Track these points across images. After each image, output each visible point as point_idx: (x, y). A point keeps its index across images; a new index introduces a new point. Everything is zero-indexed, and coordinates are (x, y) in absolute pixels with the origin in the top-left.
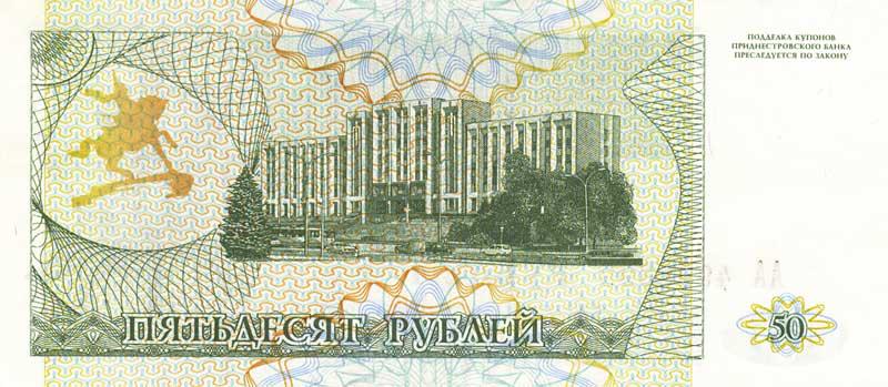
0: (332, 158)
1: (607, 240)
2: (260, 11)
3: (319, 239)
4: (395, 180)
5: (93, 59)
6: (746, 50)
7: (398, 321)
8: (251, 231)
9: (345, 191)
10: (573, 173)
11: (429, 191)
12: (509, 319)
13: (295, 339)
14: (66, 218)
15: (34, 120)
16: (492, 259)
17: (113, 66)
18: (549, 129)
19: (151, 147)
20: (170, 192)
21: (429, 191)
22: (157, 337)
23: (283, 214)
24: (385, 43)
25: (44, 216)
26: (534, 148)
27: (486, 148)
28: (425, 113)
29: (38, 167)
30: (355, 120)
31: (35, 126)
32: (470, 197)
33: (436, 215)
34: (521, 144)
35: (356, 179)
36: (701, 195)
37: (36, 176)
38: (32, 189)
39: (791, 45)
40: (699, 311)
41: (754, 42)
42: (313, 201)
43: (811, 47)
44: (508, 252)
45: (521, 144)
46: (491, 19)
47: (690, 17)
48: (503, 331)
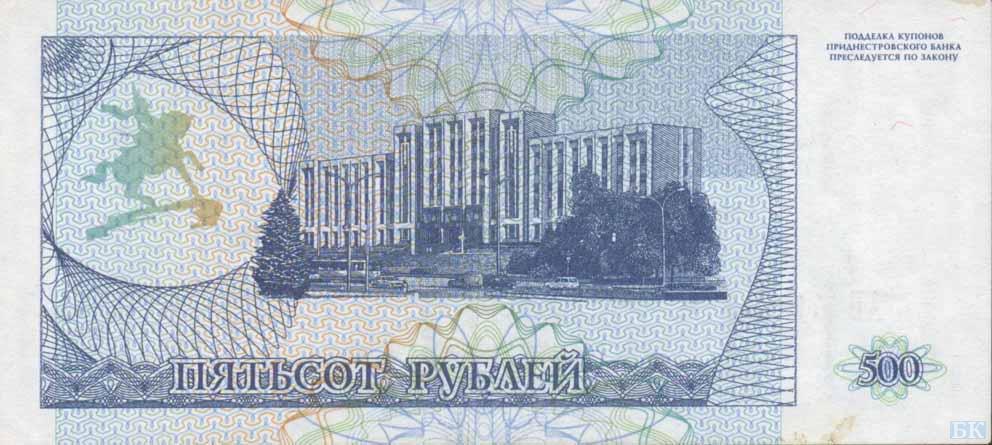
3: (364, 272)
4: (448, 204)
8: (288, 265)
10: (649, 192)
15: (45, 137)
16: (556, 293)
18: (621, 145)
19: (174, 170)
20: (196, 221)
26: (604, 166)
27: (550, 167)
28: (482, 126)
32: (534, 223)
34: (590, 162)
45: (590, 162)
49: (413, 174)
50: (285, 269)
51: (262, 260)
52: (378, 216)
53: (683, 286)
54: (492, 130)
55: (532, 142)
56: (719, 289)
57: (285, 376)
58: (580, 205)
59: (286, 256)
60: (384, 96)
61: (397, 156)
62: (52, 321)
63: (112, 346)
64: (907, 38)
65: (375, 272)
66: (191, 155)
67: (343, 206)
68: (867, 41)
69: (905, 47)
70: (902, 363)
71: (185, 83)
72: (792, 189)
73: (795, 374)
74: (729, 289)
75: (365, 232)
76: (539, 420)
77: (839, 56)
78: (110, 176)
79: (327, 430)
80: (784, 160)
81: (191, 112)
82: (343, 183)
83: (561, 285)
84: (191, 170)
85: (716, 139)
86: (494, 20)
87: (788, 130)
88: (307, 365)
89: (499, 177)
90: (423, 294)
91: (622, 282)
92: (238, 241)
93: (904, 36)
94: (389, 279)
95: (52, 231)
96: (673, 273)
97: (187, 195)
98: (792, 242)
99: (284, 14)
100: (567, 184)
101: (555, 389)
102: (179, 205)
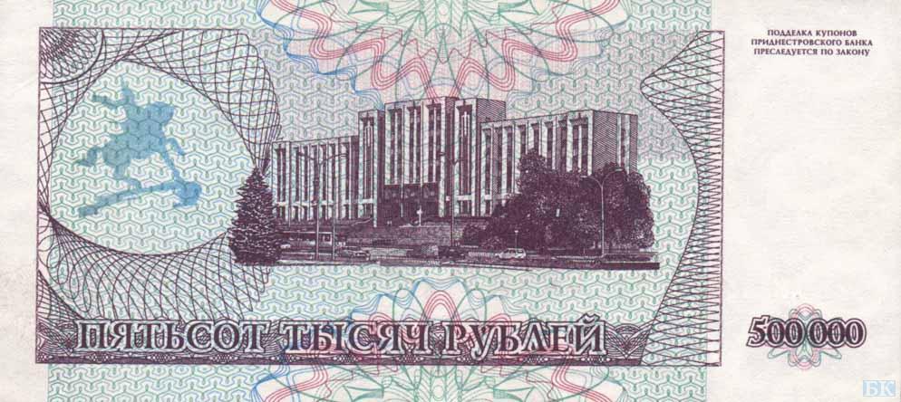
0: (344, 160)
1: (623, 243)
2: (272, 13)
3: (330, 243)
4: (407, 182)
5: (102, 57)
6: (765, 46)
7: (456, 328)
8: (262, 236)
9: (357, 193)
10: (590, 173)
11: (442, 191)
12: (571, 326)
13: (201, 346)
14: (68, 219)
15: (42, 119)
16: (505, 263)
17: (123, 65)
18: (565, 129)
19: (158, 155)
20: (177, 202)
21: (442, 191)
22: (109, 344)
23: (293, 217)
24: (399, 45)
25: (51, 220)
26: (550, 149)
27: (500, 149)
28: (439, 112)
29: (46, 168)
30: (367, 120)
31: (43, 126)
32: (483, 200)
33: (448, 218)
34: (536, 145)
35: (368, 180)
36: (720, 196)
37: (43, 177)
38: (39, 191)
39: (811, 41)
40: (716, 317)
41: (774, 38)
42: (324, 203)
43: (832, 42)
44: (523, 256)
45: (536, 145)
46: (505, 22)
47: (708, 20)
48: (565, 338)
49: (376, 160)
50: (259, 239)
51: (237, 231)
52: (344, 193)
53: (619, 257)
54: (448, 116)
55: (485, 126)
56: (652, 261)
57: (326, 338)
58: (527, 184)
59: (260, 228)
60: (350, 88)
61: (361, 139)
62: (47, 285)
63: (101, 309)
64: (824, 35)
65: (340, 243)
66: (174, 142)
67: (312, 184)
68: (788, 37)
69: (822, 43)
70: (788, 328)
71: (168, 70)
72: (719, 170)
73: (721, 337)
74: (662, 261)
75: (332, 206)
76: (488, 383)
77: (763, 50)
78: (100, 160)
79: (294, 390)
80: (712, 143)
81: (174, 103)
82: (312, 162)
83: (508, 256)
84: (173, 155)
85: (651, 123)
86: (451, 21)
87: (715, 117)
88: (199, 327)
89: (454, 159)
90: (386, 263)
91: (563, 253)
92: (218, 213)
93: (821, 33)
94: (352, 249)
95: (47, 203)
96: (611, 245)
97: (170, 177)
98: (718, 218)
99: (260, 15)
100: (516, 162)
101: (577, 350)
102: (162, 187)
